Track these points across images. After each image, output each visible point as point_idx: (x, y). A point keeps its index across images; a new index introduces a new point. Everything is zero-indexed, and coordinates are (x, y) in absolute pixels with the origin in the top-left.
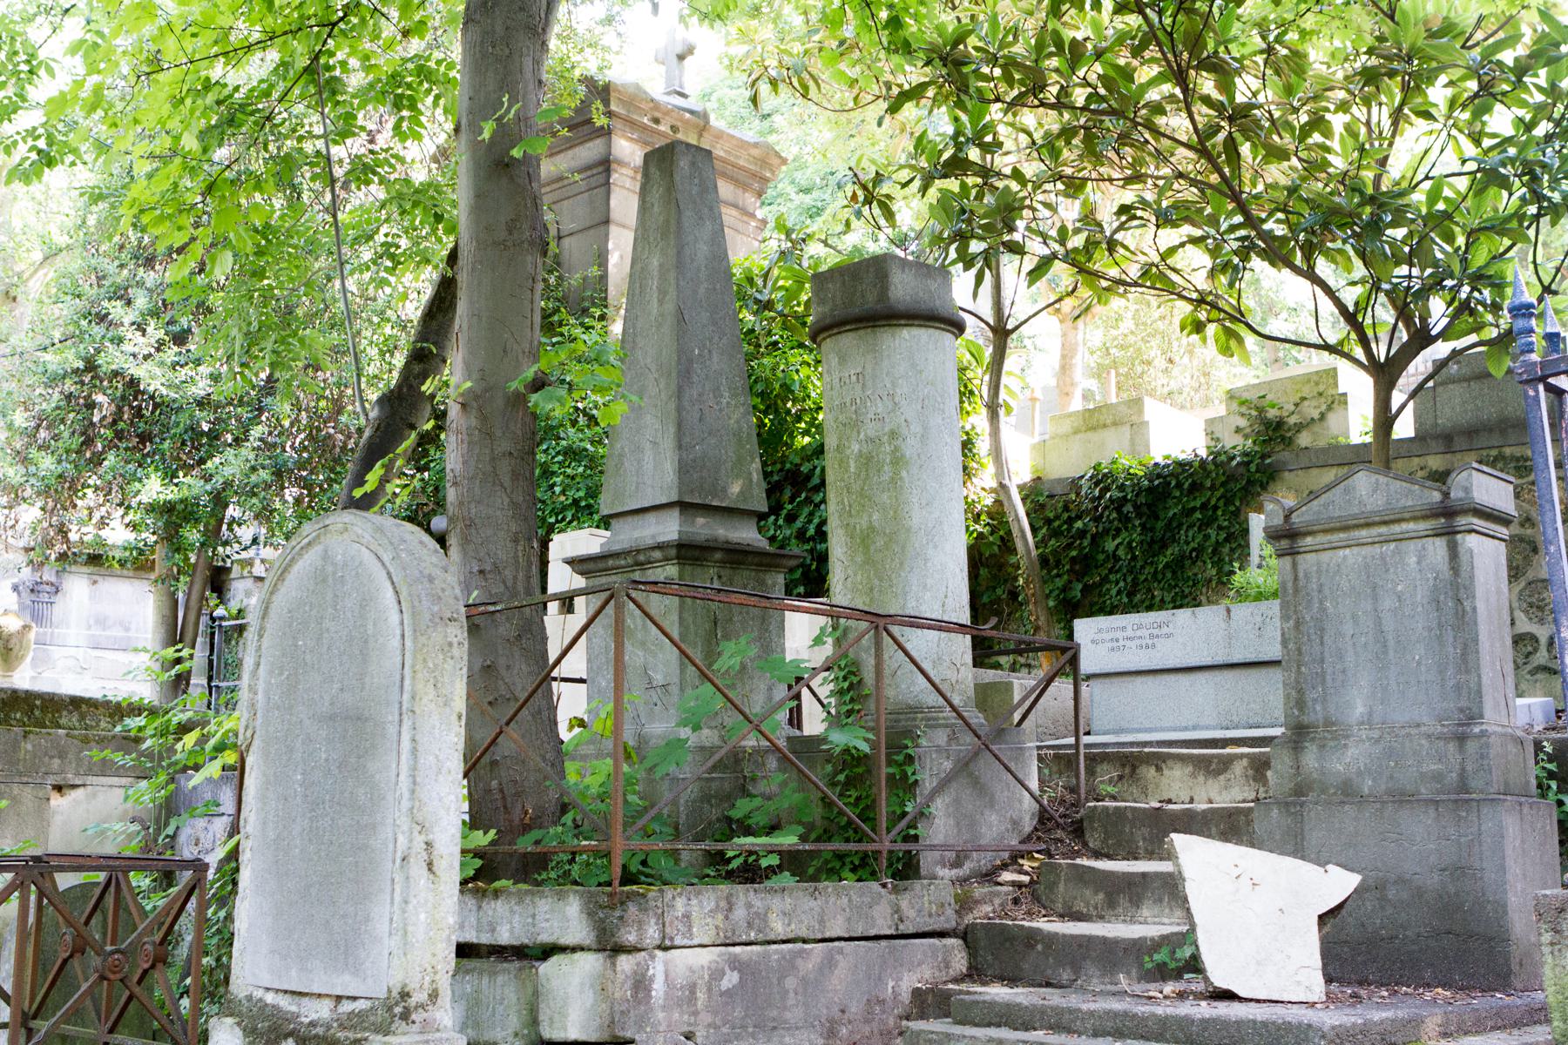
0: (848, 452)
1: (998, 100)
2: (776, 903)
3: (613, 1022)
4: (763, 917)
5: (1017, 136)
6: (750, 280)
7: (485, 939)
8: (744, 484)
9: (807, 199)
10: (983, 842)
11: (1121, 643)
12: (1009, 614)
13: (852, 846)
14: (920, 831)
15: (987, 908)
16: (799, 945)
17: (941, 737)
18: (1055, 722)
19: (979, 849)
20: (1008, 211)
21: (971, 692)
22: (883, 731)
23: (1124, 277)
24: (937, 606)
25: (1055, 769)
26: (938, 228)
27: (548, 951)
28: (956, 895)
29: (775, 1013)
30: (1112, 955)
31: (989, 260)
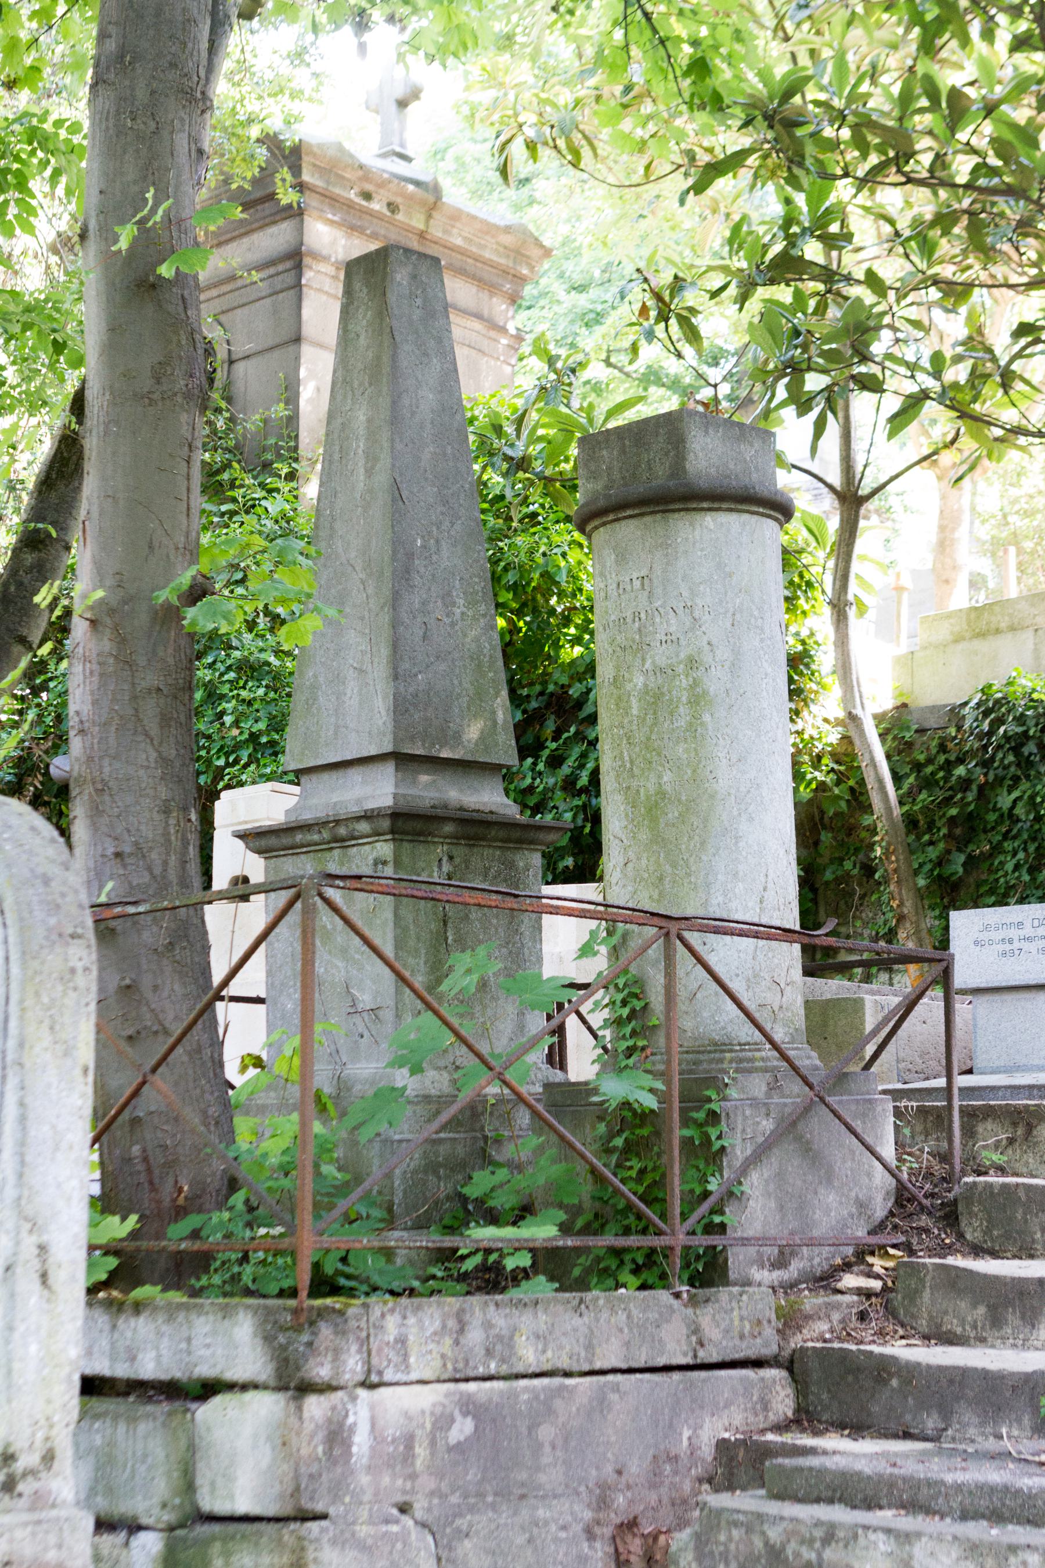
0: (629, 686)
1: (846, 175)
2: (528, 1322)
3: (297, 1489)
4: (508, 1341)
5: (874, 223)
6: (498, 429)
7: (121, 1371)
8: (486, 725)
9: (582, 301)
10: (816, 1233)
11: (1016, 945)
12: (862, 897)
13: (633, 1241)
14: (729, 1217)
15: (822, 1327)
16: (557, 1381)
17: (757, 1086)
18: (923, 1054)
19: (811, 1243)
20: (860, 331)
21: (801, 1022)
22: (676, 1078)
23: (1024, 422)
24: (752, 903)
25: (919, 1128)
26: (762, 356)
27: (209, 1389)
28: (778, 1308)
29: (523, 1476)
30: (997, 1396)
31: (833, 399)
